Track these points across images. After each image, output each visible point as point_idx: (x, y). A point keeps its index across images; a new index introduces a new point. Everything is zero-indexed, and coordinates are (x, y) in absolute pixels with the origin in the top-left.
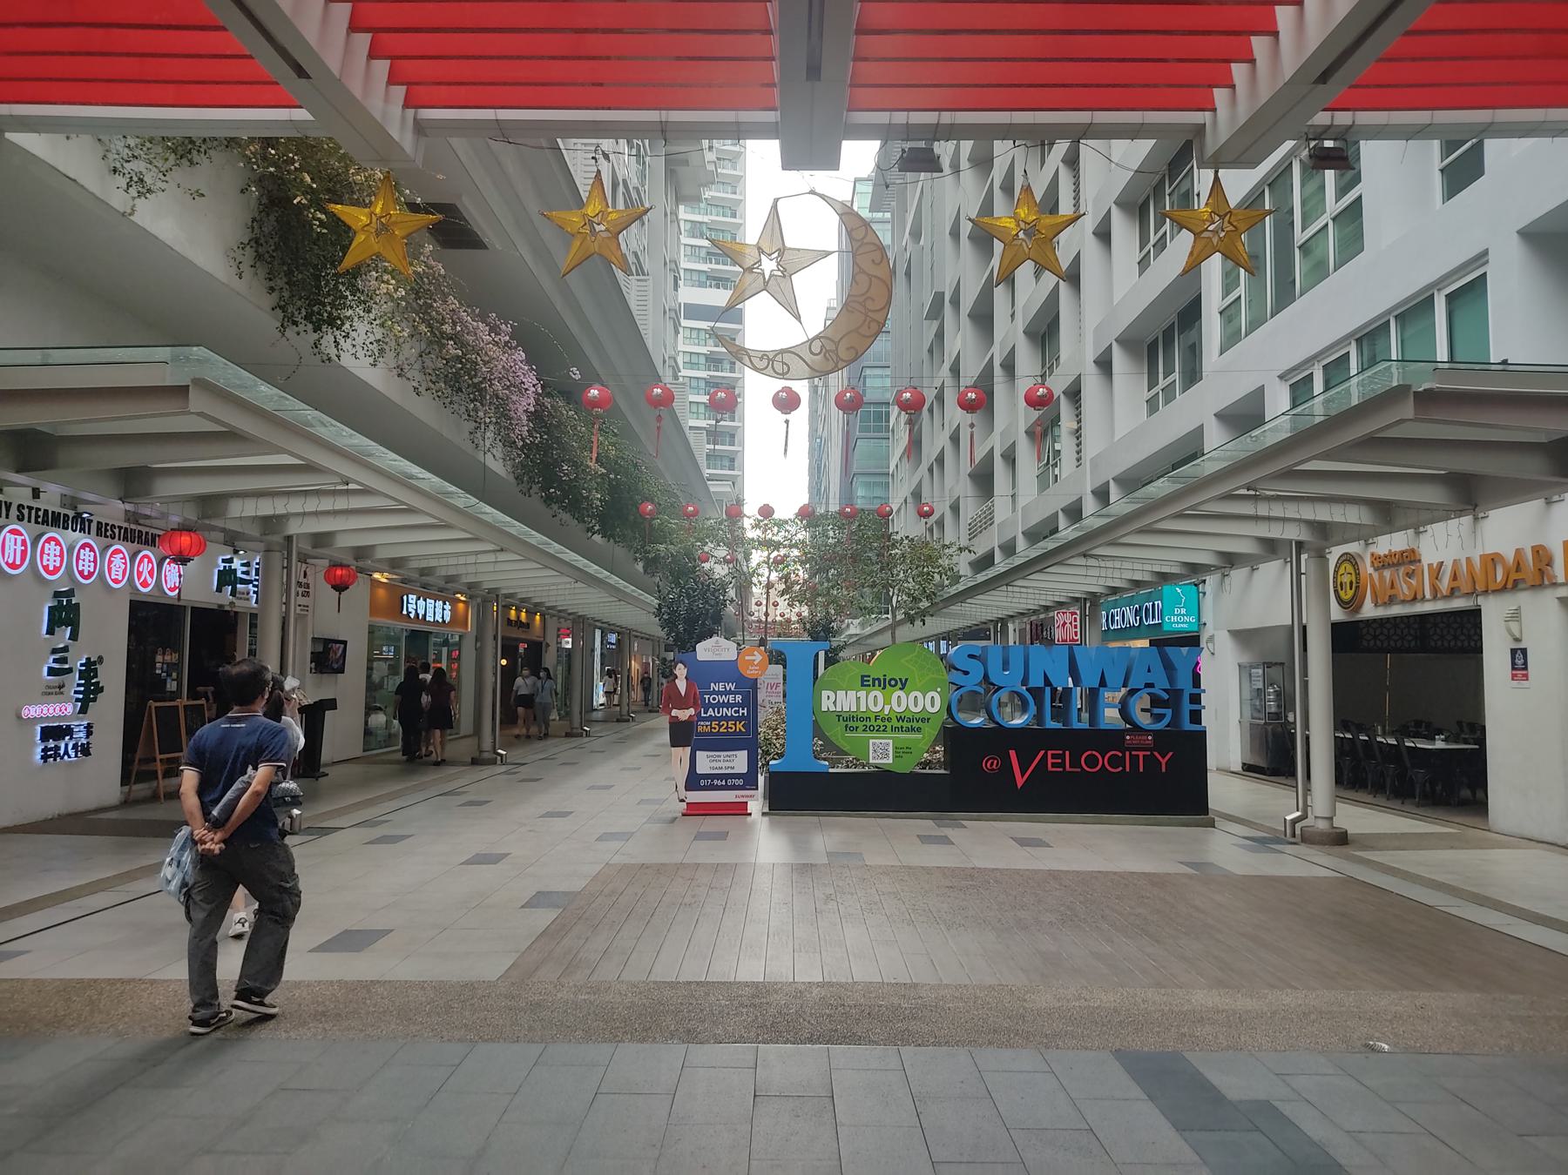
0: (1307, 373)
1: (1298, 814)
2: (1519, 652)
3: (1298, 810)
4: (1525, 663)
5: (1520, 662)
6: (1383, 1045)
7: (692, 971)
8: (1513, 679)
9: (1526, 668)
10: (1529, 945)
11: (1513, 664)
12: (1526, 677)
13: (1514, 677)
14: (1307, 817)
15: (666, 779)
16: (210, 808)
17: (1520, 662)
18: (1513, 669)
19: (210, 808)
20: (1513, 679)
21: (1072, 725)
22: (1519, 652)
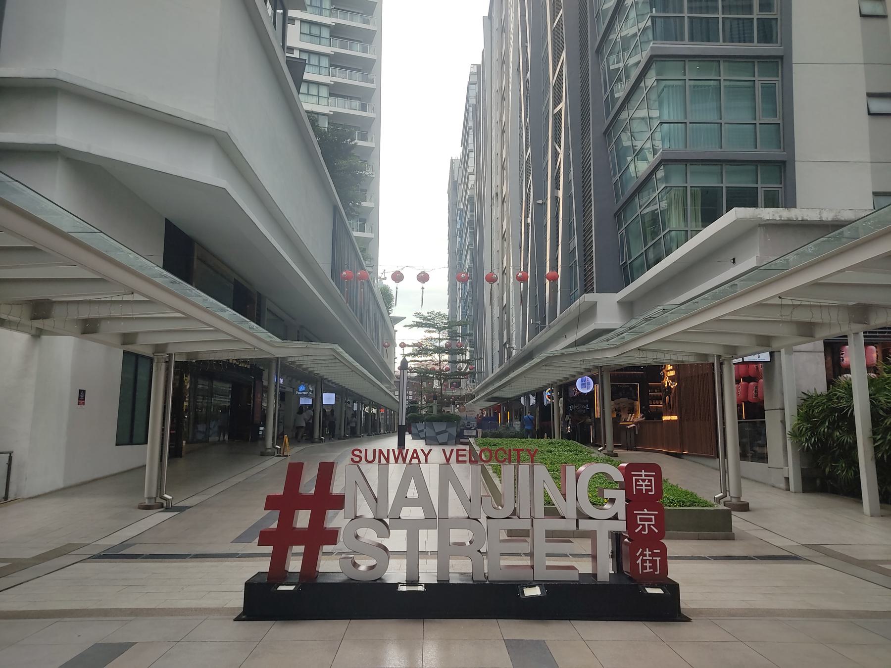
1: (722, 494)
2: (82, 392)
3: (721, 492)
4: (84, 397)
9: (84, 400)
18: (79, 399)
22: (82, 392)
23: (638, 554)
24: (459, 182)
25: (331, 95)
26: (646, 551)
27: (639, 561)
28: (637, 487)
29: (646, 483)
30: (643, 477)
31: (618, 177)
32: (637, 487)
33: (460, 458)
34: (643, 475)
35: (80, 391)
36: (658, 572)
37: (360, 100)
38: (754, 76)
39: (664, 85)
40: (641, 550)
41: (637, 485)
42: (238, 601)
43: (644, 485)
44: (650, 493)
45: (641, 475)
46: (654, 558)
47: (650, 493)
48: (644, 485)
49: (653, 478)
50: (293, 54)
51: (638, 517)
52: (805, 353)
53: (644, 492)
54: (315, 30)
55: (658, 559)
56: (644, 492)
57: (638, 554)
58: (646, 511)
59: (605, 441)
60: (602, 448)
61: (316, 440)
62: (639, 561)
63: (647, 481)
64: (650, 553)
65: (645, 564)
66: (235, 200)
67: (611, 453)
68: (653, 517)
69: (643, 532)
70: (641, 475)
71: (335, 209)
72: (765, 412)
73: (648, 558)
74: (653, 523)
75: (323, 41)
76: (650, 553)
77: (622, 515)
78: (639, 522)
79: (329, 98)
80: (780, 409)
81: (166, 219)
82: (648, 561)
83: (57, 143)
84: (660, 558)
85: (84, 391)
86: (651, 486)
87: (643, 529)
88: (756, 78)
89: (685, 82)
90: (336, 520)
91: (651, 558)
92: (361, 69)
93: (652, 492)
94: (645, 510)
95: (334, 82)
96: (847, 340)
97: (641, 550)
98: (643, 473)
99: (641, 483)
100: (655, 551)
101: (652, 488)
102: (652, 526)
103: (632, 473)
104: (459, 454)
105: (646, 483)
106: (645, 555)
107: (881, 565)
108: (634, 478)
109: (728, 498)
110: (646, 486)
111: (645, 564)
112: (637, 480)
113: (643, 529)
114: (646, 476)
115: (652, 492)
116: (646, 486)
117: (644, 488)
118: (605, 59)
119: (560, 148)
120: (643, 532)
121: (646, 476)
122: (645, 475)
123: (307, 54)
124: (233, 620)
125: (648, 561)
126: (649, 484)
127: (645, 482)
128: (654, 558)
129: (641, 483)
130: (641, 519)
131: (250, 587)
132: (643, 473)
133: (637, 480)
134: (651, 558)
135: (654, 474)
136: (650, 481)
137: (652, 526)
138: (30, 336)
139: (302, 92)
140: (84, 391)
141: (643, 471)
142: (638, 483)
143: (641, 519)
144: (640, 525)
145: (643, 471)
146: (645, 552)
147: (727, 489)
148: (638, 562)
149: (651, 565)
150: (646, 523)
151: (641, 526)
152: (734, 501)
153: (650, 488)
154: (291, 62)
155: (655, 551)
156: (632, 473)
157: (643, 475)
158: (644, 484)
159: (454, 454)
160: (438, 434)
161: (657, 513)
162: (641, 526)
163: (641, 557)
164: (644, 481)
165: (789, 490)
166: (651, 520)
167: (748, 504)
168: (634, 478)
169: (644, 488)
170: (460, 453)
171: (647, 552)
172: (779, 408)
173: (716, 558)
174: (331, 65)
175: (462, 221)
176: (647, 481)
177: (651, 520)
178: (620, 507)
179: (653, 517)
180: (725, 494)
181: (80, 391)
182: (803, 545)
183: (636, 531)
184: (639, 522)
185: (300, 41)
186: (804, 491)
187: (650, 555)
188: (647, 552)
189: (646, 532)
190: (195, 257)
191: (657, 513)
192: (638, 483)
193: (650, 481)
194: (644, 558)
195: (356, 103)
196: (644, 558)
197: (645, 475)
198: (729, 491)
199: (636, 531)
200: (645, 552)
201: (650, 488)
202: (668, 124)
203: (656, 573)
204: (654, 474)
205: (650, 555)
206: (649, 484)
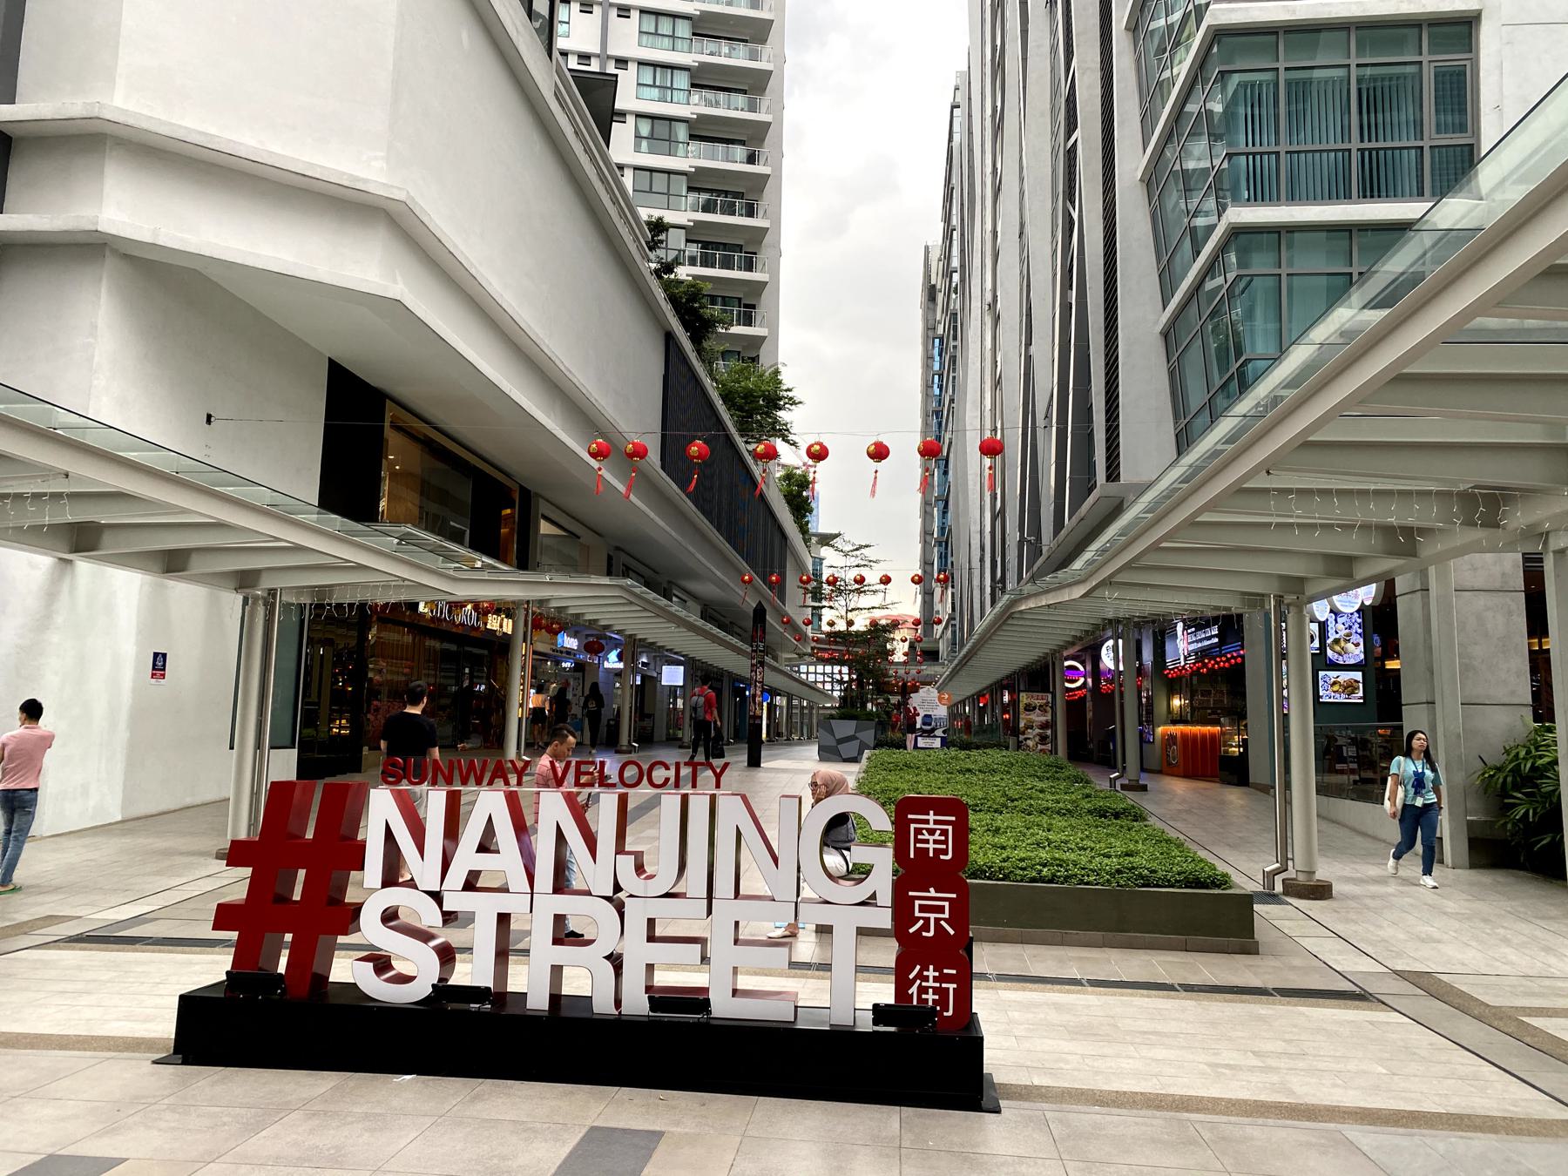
0: (644, 225)
1: (1278, 865)
2: (160, 656)
3: (1277, 862)
4: (164, 665)
5: (160, 664)
6: (400, 760)
7: (146, 576)
8: (152, 678)
9: (164, 670)
10: (436, 336)
11: (154, 665)
12: (163, 676)
13: (153, 676)
14: (1287, 870)
15: (231, 617)
16: (904, 949)
17: (160, 664)
18: (154, 669)
19: (904, 949)
20: (152, 678)
21: (142, 578)
22: (160, 656)
23: (911, 976)
24: (938, 287)
25: (692, 137)
26: (928, 970)
27: (914, 990)
28: (918, 845)
29: (937, 836)
30: (931, 826)
31: (1166, 262)
32: (918, 845)
33: (583, 779)
34: (931, 822)
35: (156, 655)
36: (950, 1013)
37: (744, 145)
38: (1421, 54)
39: (1237, 82)
40: (918, 967)
41: (917, 841)
42: (166, 1028)
43: (931, 842)
44: (942, 857)
45: (927, 822)
46: (944, 985)
47: (942, 857)
48: (931, 842)
49: (950, 828)
50: (590, 65)
51: (917, 903)
52: (1482, 593)
53: (931, 855)
54: (665, 26)
55: (952, 986)
56: (931, 855)
57: (911, 976)
58: (932, 893)
59: (1124, 761)
60: (1117, 774)
61: (624, 748)
62: (914, 990)
63: (938, 832)
64: (937, 974)
65: (924, 996)
66: (425, 323)
67: (1134, 783)
68: (946, 904)
69: (924, 934)
70: (927, 822)
71: (669, 337)
72: (1403, 707)
73: (931, 983)
74: (946, 915)
75: (679, 43)
76: (937, 974)
77: (885, 897)
78: (917, 914)
79: (688, 144)
80: (1428, 703)
81: (329, 358)
82: (931, 991)
83: (99, 229)
84: (955, 986)
85: (164, 656)
86: (945, 842)
87: (926, 927)
88: (1425, 58)
89: (1278, 74)
90: (235, 883)
91: (938, 985)
92: (746, 88)
93: (947, 854)
94: (932, 889)
95: (696, 114)
96: (1543, 567)
97: (918, 967)
98: (931, 817)
99: (927, 836)
100: (945, 971)
101: (915, 845)
102: (942, 923)
103: (910, 816)
104: (582, 770)
105: (937, 836)
106: (926, 979)
107: (1524, 1019)
108: (913, 826)
109: (1291, 874)
110: (935, 842)
111: (924, 996)
112: (918, 831)
113: (926, 927)
114: (936, 822)
115: (947, 854)
116: (935, 842)
117: (931, 846)
118: (1141, 42)
119: (1074, 209)
120: (924, 934)
121: (936, 822)
122: (929, 824)
123: (652, 68)
124: (150, 1062)
125: (931, 991)
126: (943, 838)
127: (933, 834)
128: (944, 985)
129: (927, 836)
130: (923, 909)
131: (190, 1005)
132: (931, 817)
133: (918, 831)
134: (938, 985)
135: (953, 818)
136: (944, 833)
137: (942, 923)
138: (57, 560)
139: (668, 135)
140: (164, 656)
141: (931, 812)
142: (920, 837)
143: (923, 909)
144: (919, 918)
145: (931, 812)
146: (925, 973)
147: (1290, 856)
148: (910, 992)
149: (937, 997)
150: (932, 916)
151: (921, 922)
152: (1302, 878)
153: (944, 847)
154: (584, 81)
155: (945, 971)
156: (910, 816)
157: (931, 822)
158: (931, 838)
159: (572, 771)
160: (841, 741)
161: (954, 896)
162: (921, 922)
163: (918, 982)
164: (931, 832)
165: (1443, 863)
166: (941, 910)
167: (1331, 886)
168: (913, 826)
169: (931, 846)
170: (583, 768)
171: (931, 973)
172: (1425, 701)
173: (1189, 988)
174: (693, 85)
175: (941, 359)
176: (938, 832)
177: (941, 910)
178: (882, 881)
179: (946, 904)
180: (1284, 863)
181: (156, 655)
182: (1395, 972)
183: (911, 931)
184: (917, 914)
185: (639, 45)
186: (1474, 865)
187: (936, 979)
188: (931, 973)
189: (931, 934)
190: (387, 424)
191: (954, 896)
192: (920, 837)
193: (944, 833)
194: (924, 984)
195: (739, 152)
196: (924, 984)
197: (929, 824)
198: (1293, 859)
199: (911, 931)
200: (925, 973)
201: (944, 847)
202: (607, 72)
203: (945, 1014)
204: (953, 818)
205: (936, 979)
206: (943, 838)
